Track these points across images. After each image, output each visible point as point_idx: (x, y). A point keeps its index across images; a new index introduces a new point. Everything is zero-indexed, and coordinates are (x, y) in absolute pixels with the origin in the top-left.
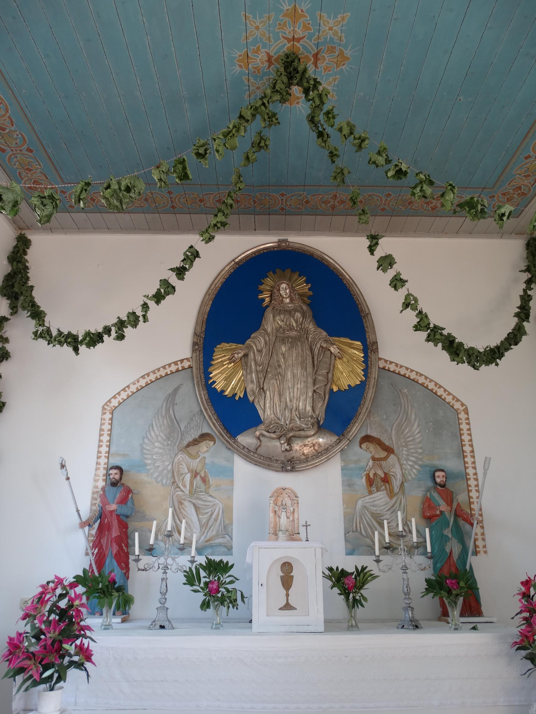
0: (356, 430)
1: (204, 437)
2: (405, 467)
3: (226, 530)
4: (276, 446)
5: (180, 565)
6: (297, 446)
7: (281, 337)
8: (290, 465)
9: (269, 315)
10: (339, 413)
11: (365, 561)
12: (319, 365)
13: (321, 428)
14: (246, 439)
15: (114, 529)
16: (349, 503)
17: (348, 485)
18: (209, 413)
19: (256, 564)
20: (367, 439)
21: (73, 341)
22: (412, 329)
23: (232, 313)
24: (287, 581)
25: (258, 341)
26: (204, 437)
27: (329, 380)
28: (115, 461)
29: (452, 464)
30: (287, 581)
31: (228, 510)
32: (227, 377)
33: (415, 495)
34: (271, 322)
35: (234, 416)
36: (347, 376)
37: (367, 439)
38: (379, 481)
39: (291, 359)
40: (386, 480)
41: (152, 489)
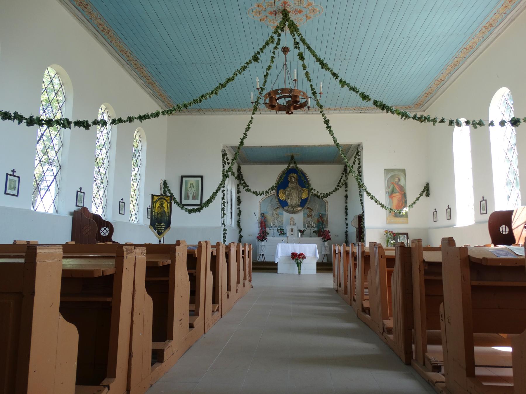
0: (306, 206)
1: (278, 208)
2: (315, 213)
3: (282, 224)
4: (291, 209)
5: (238, 183)
6: (295, 209)
7: (292, 188)
8: (294, 213)
9: (290, 184)
10: (303, 203)
11: (305, 229)
12: (299, 195)
13: (299, 206)
14: (286, 208)
15: (263, 223)
16: (304, 219)
17: (304, 216)
18: (278, 203)
19: (287, 229)
20: (308, 208)
21: (255, 193)
22: (504, 127)
23: (282, 184)
24: (292, 231)
25: (288, 189)
26: (278, 208)
27: (301, 197)
28: (262, 212)
29: (323, 212)
30: (292, 231)
31: (283, 221)
32: (282, 196)
33: (316, 218)
34: (290, 185)
35: (283, 204)
36: (304, 196)
37: (308, 208)
38: (310, 216)
39: (294, 193)
40: (311, 215)
41: (269, 217)
